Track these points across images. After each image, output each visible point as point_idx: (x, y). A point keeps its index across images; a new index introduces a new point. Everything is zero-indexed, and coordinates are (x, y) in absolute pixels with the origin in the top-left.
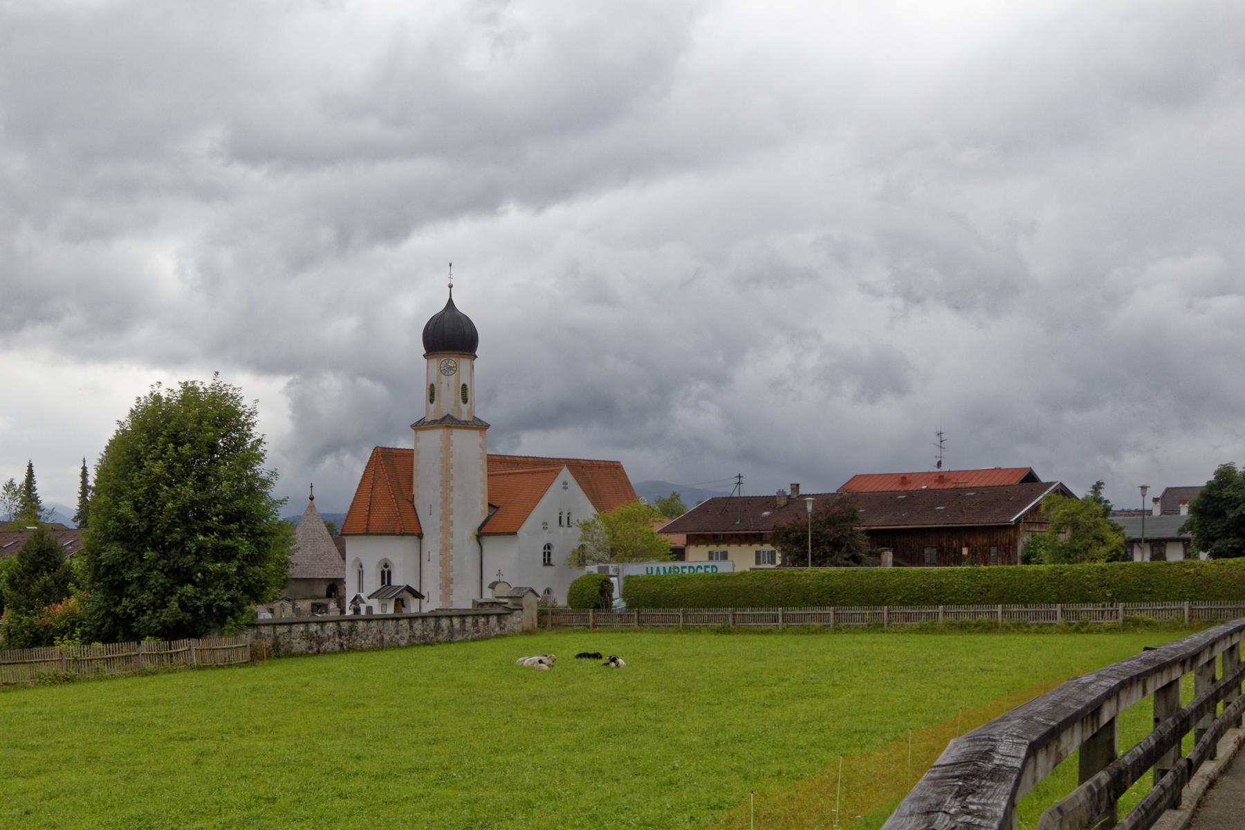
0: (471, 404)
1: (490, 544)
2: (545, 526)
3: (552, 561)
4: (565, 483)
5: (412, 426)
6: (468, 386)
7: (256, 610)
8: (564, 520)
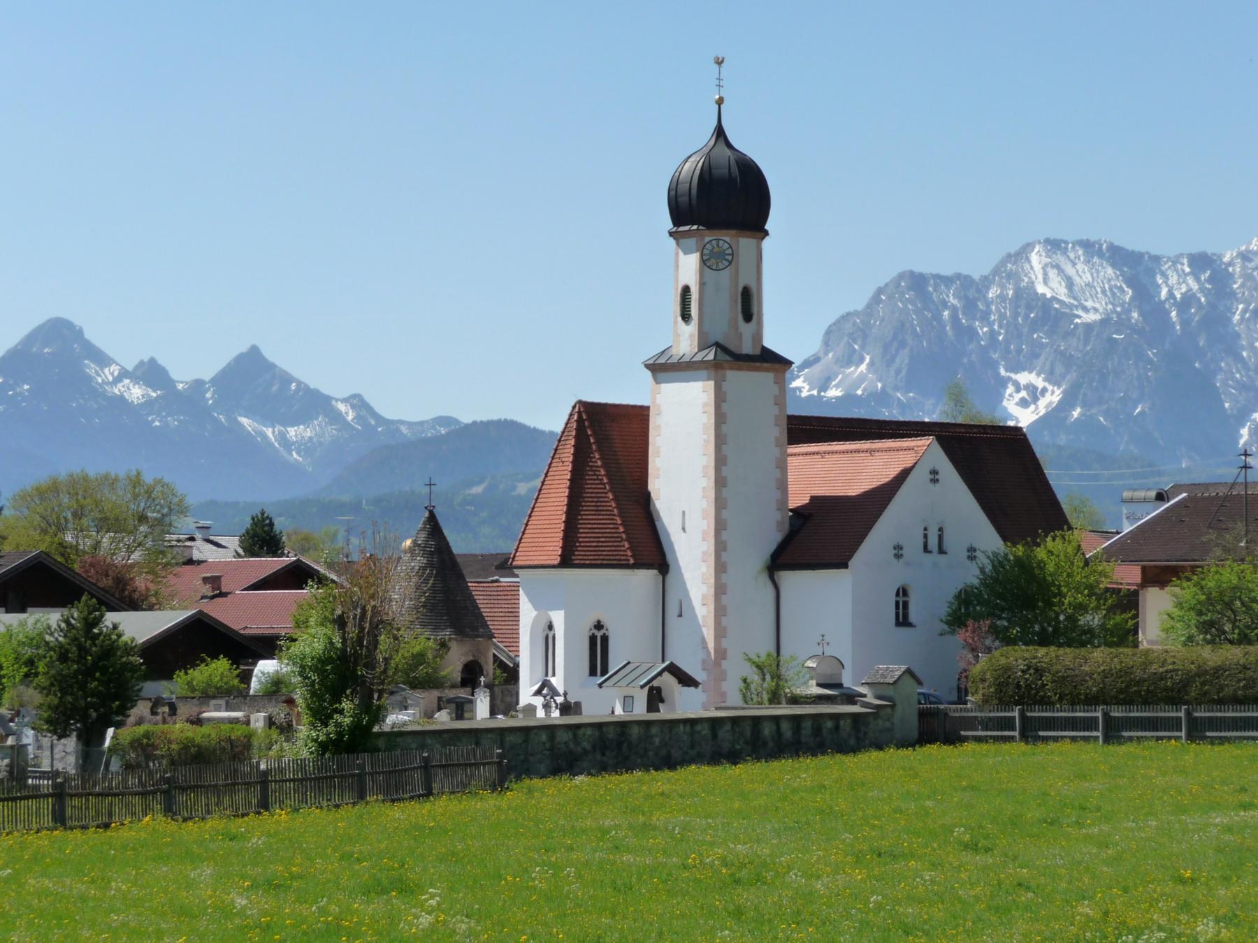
1: (792, 580)
2: (898, 552)
4: (934, 472)
8: (933, 543)
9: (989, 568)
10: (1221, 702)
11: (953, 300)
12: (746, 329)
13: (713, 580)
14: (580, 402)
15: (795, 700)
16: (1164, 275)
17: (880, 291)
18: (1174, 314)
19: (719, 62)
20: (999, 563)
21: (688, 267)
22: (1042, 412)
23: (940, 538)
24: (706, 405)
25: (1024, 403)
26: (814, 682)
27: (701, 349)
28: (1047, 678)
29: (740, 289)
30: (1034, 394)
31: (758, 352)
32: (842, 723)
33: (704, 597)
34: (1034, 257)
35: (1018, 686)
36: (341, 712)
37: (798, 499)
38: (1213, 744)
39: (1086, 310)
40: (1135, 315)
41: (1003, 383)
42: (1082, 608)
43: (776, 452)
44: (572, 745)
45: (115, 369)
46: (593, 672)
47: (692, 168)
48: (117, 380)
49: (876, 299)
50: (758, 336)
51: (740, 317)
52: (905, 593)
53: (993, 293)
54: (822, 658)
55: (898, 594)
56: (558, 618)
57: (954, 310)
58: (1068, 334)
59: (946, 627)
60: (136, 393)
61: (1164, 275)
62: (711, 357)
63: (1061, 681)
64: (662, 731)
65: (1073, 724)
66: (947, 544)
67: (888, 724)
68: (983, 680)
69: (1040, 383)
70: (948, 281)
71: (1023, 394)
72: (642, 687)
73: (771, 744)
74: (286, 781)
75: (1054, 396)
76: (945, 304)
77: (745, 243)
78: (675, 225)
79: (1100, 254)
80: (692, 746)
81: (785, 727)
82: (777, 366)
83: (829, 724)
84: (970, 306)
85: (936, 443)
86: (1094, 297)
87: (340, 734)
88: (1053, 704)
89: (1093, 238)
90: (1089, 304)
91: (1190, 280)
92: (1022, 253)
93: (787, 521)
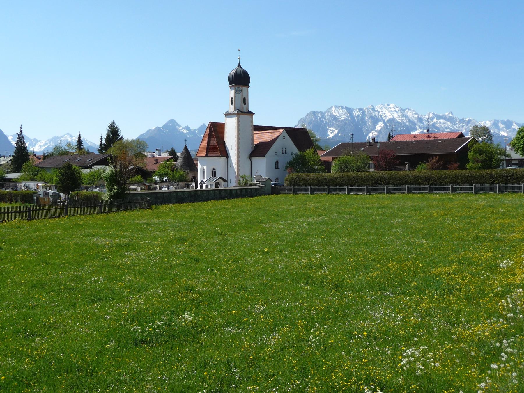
1: (255, 160)
8: (284, 152)
9: (294, 157)
10: (337, 185)
11: (319, 116)
12: (245, 106)
13: (237, 160)
14: (210, 122)
15: (251, 185)
16: (354, 112)
17: (308, 114)
18: (356, 118)
19: (239, 50)
20: (297, 155)
21: (232, 93)
22: (334, 134)
23: (285, 151)
24: (235, 122)
25: (331, 133)
26: (256, 181)
27: (235, 111)
28: (300, 180)
30: (333, 131)
31: (247, 111)
32: (253, 190)
33: (235, 163)
34: (333, 108)
35: (294, 182)
36: (114, 189)
37: (256, 142)
38: (333, 194)
39: (341, 117)
40: (350, 118)
41: (328, 129)
42: (313, 165)
43: (251, 132)
44: (182, 196)
45: (181, 127)
47: (233, 72)
48: (182, 129)
49: (307, 115)
50: (247, 108)
51: (243, 104)
52: (278, 162)
53: (326, 114)
54: (258, 176)
55: (276, 162)
56: (205, 167)
57: (320, 117)
58: (339, 121)
59: (285, 169)
60: (185, 131)
61: (354, 112)
62: (236, 112)
63: (303, 180)
65: (304, 190)
67: (264, 190)
68: (287, 180)
69: (334, 129)
70: (319, 112)
71: (331, 131)
72: (214, 182)
73: (235, 195)
74: (42, 210)
75: (336, 132)
76: (318, 116)
77: (244, 88)
78: (230, 84)
79: (344, 108)
80: (214, 196)
81: (238, 191)
83: (249, 190)
84: (322, 117)
85: (285, 131)
86: (343, 115)
87: (114, 194)
88: (302, 185)
89: (343, 105)
90: (342, 116)
91: (359, 112)
92: (331, 108)
93: (253, 148)
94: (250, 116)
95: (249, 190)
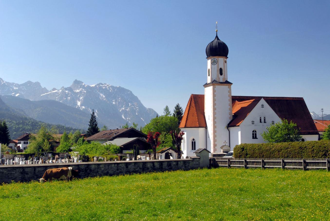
0: (224, 75)
1: (232, 129)
2: (253, 122)
3: (257, 137)
4: (263, 105)
5: (204, 86)
6: (223, 69)
7: (39, 139)
8: (263, 120)
13: (213, 130)
14: (192, 94)
23: (265, 120)
29: (219, 69)
31: (224, 81)
32: (179, 163)
46: (193, 149)
52: (255, 132)
64: (105, 166)
66: (266, 121)
67: (197, 163)
80: (118, 170)
82: (228, 84)
94: (227, 86)
95: (174, 163)
